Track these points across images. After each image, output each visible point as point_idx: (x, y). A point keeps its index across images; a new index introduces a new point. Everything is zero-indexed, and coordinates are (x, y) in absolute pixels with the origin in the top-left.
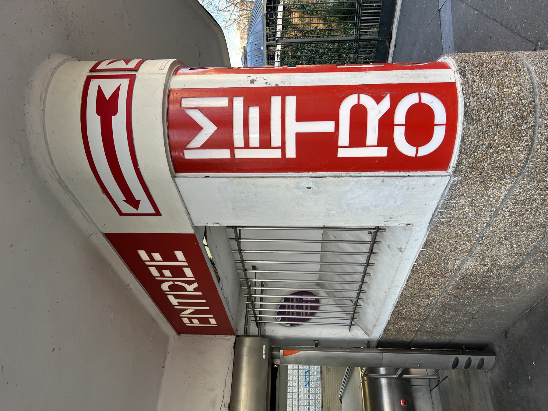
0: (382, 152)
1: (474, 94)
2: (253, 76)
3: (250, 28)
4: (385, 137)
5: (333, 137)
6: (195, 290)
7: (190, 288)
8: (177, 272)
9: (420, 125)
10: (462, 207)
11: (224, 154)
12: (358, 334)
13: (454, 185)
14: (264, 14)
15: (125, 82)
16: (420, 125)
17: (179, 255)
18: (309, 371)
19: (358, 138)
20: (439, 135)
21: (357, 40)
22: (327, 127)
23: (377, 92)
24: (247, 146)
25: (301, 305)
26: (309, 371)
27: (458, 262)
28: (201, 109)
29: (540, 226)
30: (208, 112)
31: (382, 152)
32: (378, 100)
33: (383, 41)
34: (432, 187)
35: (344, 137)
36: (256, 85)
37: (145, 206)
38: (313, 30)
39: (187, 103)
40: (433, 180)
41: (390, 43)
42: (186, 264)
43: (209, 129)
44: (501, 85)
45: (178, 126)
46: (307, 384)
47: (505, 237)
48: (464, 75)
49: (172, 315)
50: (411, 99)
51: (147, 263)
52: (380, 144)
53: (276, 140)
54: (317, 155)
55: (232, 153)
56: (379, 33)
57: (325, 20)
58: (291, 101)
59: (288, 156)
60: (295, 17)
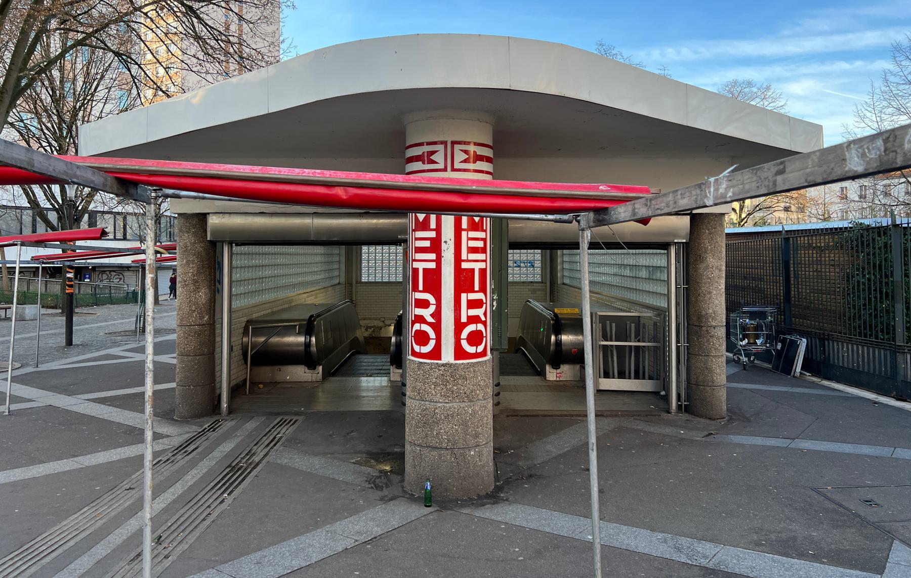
0: (464, 319)
1: (431, 369)
5: (473, 291)
18: (533, 266)
19: (472, 304)
31: (464, 319)
32: (432, 315)
35: (473, 296)
48: (443, 365)
50: (432, 335)
52: (469, 317)
55: (465, 230)
58: (433, 265)
59: (434, 258)
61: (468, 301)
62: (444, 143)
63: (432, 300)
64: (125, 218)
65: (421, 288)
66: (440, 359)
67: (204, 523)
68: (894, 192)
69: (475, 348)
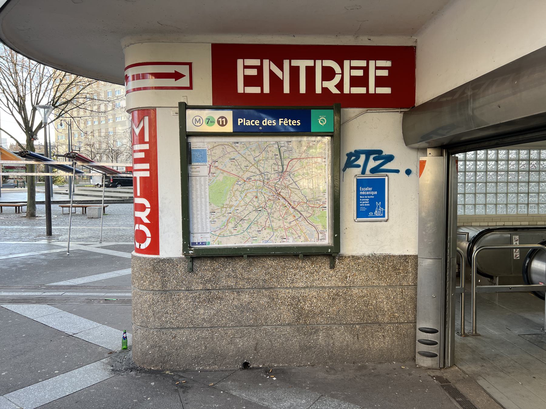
50: (148, 233)
58: (147, 174)
63: (148, 204)
64: (135, 151)
65: (139, 194)
67: (84, 246)
68: (256, 123)
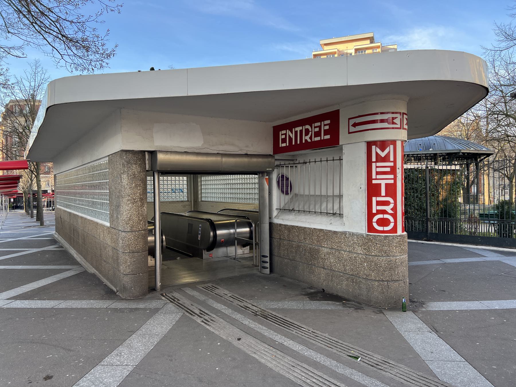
0: (374, 211)
1: (393, 238)
2: (400, 169)
3: (448, 138)
4: (379, 212)
5: (380, 195)
6: (306, 140)
7: (308, 138)
8: (318, 134)
9: (383, 222)
10: (353, 240)
11: (374, 159)
12: (275, 213)
13: (362, 235)
14: (460, 150)
15: (399, 126)
16: (383, 222)
17: (328, 137)
18: (183, 192)
19: (379, 203)
20: (380, 228)
21: (427, 220)
22: (383, 193)
23: (395, 209)
24: (377, 167)
25: (285, 185)
26: (183, 192)
27: (326, 246)
28: (389, 152)
29: (345, 268)
30: (388, 154)
32: (392, 209)
33: (427, 236)
34: (362, 229)
35: (379, 199)
36: (397, 170)
37: (352, 129)
38: (438, 191)
39: (392, 147)
40: (364, 228)
41: (425, 240)
42: (322, 139)
43: (383, 154)
44: (396, 247)
45: (383, 145)
46: (174, 191)
47: (339, 259)
48: (399, 236)
49: (290, 126)
50: (392, 219)
51: (323, 122)
53: (379, 177)
54: (373, 190)
55: (374, 162)
56: (431, 233)
57: (445, 200)
58: (392, 182)
59: (373, 181)
60: (448, 178)
61: (377, 201)
62: (400, 113)
66: (397, 233)
69: (382, 227)
